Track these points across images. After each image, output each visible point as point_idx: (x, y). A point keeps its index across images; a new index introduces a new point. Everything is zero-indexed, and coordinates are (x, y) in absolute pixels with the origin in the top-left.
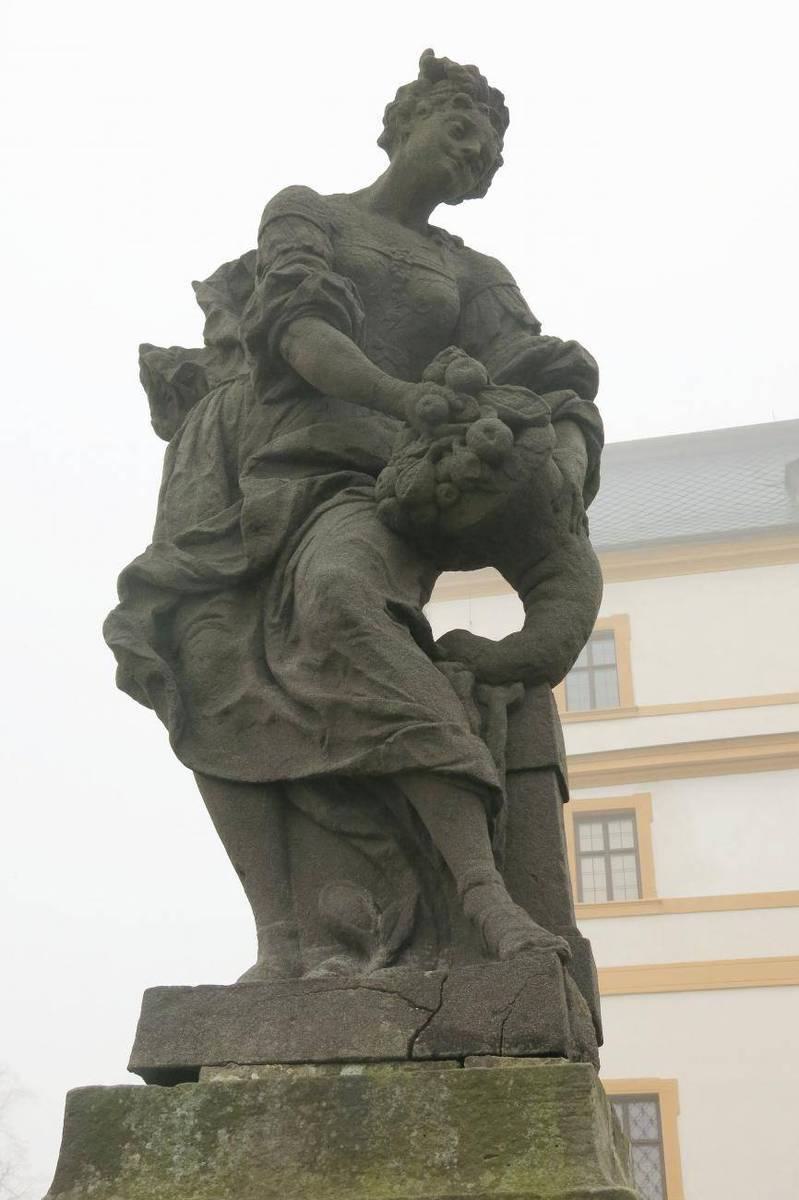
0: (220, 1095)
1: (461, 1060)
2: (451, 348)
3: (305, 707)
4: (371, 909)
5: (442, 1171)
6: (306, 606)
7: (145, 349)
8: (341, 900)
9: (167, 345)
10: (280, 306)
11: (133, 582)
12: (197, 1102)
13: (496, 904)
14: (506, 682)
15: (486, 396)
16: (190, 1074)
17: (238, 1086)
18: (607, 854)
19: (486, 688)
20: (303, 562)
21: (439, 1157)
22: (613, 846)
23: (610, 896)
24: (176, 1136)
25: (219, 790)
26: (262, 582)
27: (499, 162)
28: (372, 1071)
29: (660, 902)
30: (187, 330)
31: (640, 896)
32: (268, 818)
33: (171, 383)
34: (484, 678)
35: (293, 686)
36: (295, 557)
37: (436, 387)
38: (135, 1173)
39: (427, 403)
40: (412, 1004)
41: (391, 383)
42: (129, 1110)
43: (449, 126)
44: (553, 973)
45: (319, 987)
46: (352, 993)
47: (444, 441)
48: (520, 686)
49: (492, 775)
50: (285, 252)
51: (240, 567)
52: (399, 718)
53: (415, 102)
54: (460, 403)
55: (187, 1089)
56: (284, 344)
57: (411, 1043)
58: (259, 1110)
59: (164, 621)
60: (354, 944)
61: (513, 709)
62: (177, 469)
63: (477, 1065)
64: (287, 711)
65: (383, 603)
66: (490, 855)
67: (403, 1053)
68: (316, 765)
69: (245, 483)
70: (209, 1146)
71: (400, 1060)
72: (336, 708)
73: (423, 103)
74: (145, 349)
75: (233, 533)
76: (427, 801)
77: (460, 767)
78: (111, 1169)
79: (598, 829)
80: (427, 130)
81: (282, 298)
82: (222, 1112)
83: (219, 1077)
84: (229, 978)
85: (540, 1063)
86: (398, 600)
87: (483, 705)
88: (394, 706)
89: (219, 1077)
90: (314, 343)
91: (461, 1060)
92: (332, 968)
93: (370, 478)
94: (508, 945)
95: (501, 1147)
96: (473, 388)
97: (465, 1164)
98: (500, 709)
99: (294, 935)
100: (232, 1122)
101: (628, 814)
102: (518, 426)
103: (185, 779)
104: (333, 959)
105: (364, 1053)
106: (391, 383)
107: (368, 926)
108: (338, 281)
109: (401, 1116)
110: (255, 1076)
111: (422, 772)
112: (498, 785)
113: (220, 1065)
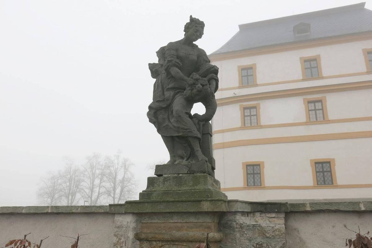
0: (165, 178)
1: (193, 174)
2: (193, 73)
3: (174, 126)
4: (184, 153)
5: (190, 186)
6: (174, 113)
7: (150, 64)
8: (180, 152)
9: (152, 63)
10: (169, 65)
11: (150, 107)
12: (163, 179)
13: (199, 153)
14: (203, 121)
15: (199, 81)
16: (162, 175)
17: (167, 177)
18: (251, 116)
19: (200, 122)
20: (174, 106)
21: (190, 185)
22: (252, 114)
23: (251, 125)
24: (161, 182)
25: (164, 137)
26: (168, 108)
27: (203, 34)
28: (183, 175)
29: (261, 126)
30: (156, 60)
31: (257, 124)
32: (171, 141)
33: (154, 70)
34: (199, 121)
35: (173, 124)
36: (173, 104)
37: (191, 79)
38: (156, 186)
39: (190, 83)
40: (188, 167)
41: (186, 78)
42: (155, 179)
43: (195, 28)
44: (204, 163)
45: (176, 165)
46: (180, 166)
47: (193, 88)
48: (204, 122)
49: (199, 136)
50: (169, 55)
51: (165, 106)
52: (186, 129)
53: (189, 26)
54: (195, 82)
55: (161, 177)
56: (170, 71)
57: (187, 172)
58: (170, 180)
59: (155, 113)
60: (182, 158)
61: (203, 125)
62: (155, 89)
63: (195, 175)
64: (172, 127)
65: (184, 113)
66: (199, 146)
67: (187, 173)
68: (176, 134)
69: (166, 93)
70: (164, 184)
71: (186, 174)
72: (178, 127)
73: (190, 26)
74: (150, 64)
75: (163, 101)
76: (190, 139)
77: (195, 136)
78: (153, 186)
79: (249, 111)
80: (191, 31)
81: (169, 64)
82: (165, 180)
83: (165, 176)
84: (166, 163)
85: (203, 174)
86: (186, 112)
87: (199, 125)
88: (186, 128)
89: (165, 176)
90: (175, 71)
91: (193, 174)
92: (179, 161)
93: (183, 91)
94: (200, 159)
95: (197, 184)
96: (197, 80)
97: (193, 186)
98: (201, 125)
99: (175, 156)
100: (167, 181)
101: (255, 107)
102: (203, 85)
103: (159, 136)
104: (180, 160)
105: (182, 173)
106: (186, 78)
107: (184, 156)
108: (178, 61)
109: (186, 180)
110: (169, 176)
111: (190, 136)
112: (201, 137)
113: (166, 174)
